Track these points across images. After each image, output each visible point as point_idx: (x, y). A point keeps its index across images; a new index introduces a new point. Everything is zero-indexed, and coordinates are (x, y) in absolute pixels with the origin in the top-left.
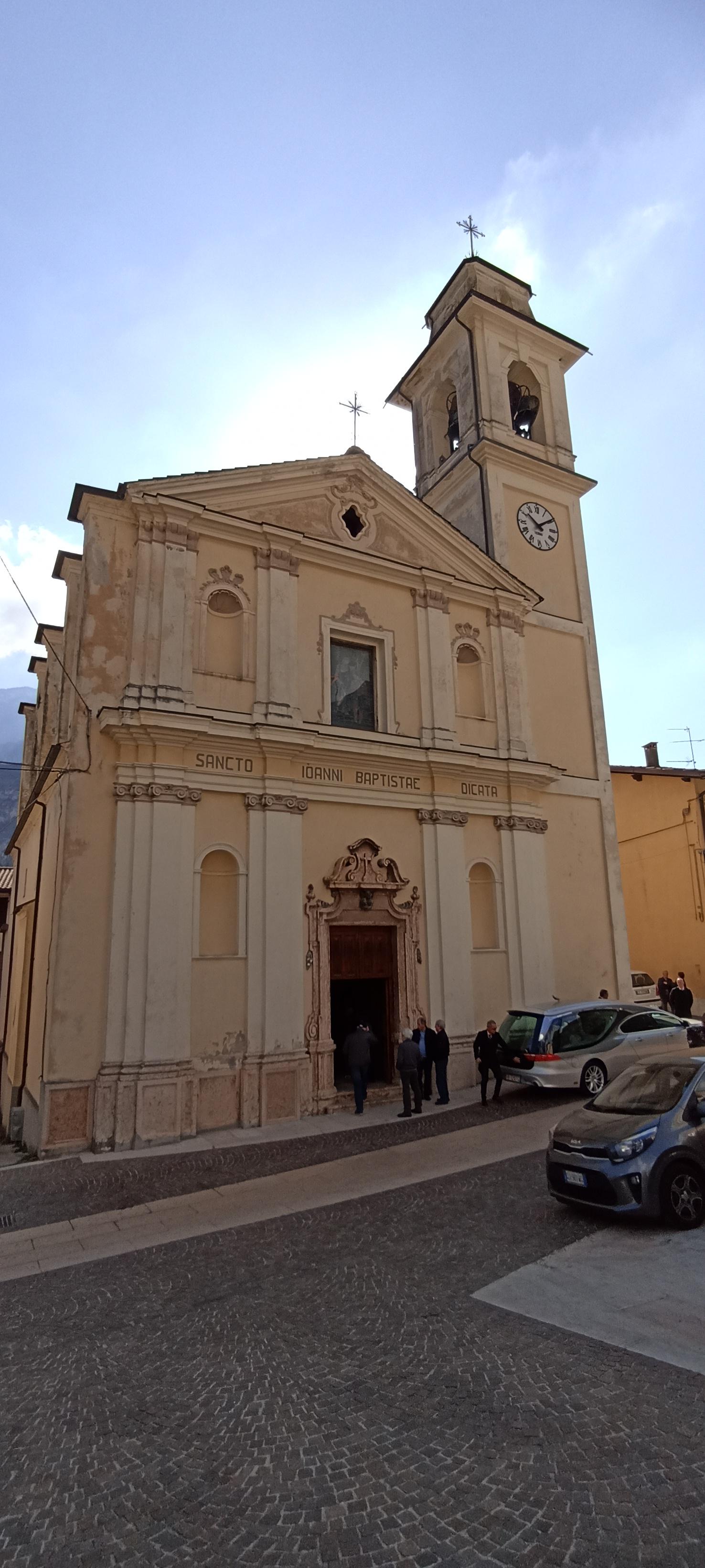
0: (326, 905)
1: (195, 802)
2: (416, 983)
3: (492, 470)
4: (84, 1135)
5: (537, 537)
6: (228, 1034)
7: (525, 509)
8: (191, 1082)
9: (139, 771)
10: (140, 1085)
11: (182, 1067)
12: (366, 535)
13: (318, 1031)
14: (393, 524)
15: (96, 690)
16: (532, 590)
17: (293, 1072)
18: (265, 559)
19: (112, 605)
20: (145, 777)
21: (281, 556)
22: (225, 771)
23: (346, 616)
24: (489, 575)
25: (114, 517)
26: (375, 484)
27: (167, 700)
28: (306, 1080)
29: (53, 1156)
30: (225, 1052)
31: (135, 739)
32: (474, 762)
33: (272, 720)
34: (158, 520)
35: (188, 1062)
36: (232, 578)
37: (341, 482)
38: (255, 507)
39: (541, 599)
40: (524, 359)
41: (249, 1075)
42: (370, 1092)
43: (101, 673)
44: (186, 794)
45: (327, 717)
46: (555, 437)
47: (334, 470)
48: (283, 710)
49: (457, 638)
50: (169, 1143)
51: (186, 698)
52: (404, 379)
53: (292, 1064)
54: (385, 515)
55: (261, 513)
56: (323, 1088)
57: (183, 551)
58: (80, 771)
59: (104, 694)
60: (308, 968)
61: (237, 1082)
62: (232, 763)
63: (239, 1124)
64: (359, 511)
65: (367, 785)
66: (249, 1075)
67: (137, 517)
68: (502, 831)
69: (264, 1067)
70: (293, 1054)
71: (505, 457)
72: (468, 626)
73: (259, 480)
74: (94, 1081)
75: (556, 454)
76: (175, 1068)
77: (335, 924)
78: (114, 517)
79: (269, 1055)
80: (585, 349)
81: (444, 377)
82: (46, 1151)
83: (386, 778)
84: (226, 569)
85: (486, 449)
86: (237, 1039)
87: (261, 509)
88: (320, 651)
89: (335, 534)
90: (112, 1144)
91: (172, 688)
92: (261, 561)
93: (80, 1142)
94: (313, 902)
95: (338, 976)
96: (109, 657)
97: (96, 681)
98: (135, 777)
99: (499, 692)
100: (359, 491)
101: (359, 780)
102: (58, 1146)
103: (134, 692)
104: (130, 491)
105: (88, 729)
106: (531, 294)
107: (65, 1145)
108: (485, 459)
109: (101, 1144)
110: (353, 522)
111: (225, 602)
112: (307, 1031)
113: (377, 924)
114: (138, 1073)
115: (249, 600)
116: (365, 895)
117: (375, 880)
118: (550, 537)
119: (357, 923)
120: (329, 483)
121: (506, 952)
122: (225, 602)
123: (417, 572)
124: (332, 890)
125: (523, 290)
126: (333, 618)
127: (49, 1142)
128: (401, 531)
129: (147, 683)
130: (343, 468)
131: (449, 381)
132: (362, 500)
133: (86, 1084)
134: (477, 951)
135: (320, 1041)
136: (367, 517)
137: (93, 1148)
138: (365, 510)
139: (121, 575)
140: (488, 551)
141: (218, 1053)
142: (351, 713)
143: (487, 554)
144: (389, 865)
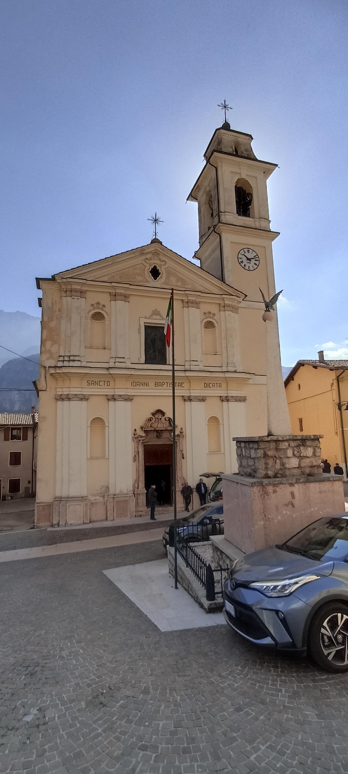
0: (142, 437)
1: (131, 400)
2: (182, 467)
3: (224, 235)
4: (50, 521)
5: (248, 265)
6: (102, 486)
7: (242, 252)
8: (87, 504)
9: (64, 389)
10: (68, 505)
11: (82, 499)
12: (161, 278)
13: (138, 485)
14: (174, 271)
15: (48, 359)
16: (241, 292)
17: (127, 501)
18: (114, 296)
19: (53, 324)
20: (66, 391)
21: (121, 295)
22: (99, 387)
23: (152, 316)
24: (220, 288)
25: (52, 288)
26: (164, 254)
27: (74, 361)
28: (132, 504)
29: (39, 528)
30: (101, 493)
31: (62, 377)
32: (208, 374)
33: (117, 365)
34: (69, 287)
35: (86, 497)
36: (101, 306)
37: (148, 256)
38: (111, 274)
39: (246, 296)
40: (244, 176)
41: (110, 502)
42: (156, 509)
43: (50, 351)
44: (82, 397)
45: (143, 359)
46: (259, 213)
47: (145, 252)
48: (122, 360)
49: (204, 319)
50: (79, 525)
51: (82, 359)
52: (192, 190)
53: (127, 498)
54: (170, 267)
55: (113, 276)
56: (140, 507)
57: (79, 299)
58: (43, 390)
59: (51, 360)
60: (134, 461)
61: (105, 504)
62: (102, 383)
63: (106, 519)
64: (158, 268)
65: (160, 387)
66: (110, 502)
67: (61, 287)
68: (224, 403)
69: (115, 499)
70: (128, 494)
71: (230, 229)
72: (210, 313)
73: (111, 263)
74: (52, 503)
75: (260, 222)
76: (81, 499)
77: (146, 444)
78: (52, 288)
79: (117, 495)
80: (277, 165)
81: (208, 190)
82: (37, 526)
83: (169, 384)
84: (98, 303)
85: (221, 227)
86: (106, 488)
87: (113, 274)
88: (139, 332)
89: (146, 280)
90: (58, 525)
91: (76, 356)
92: (222, 308)
93: (48, 523)
94: (136, 436)
95: (149, 464)
96: (52, 345)
97: (47, 355)
98: (63, 392)
99: (224, 341)
100: (158, 259)
101: (156, 385)
102: (40, 525)
103: (61, 359)
104: (57, 278)
105: (45, 374)
106: (252, 139)
107: (43, 524)
108: (221, 231)
109: (55, 525)
110: (155, 273)
111: (98, 316)
112: (134, 486)
113: (165, 443)
114: (67, 501)
115: (108, 315)
116: (159, 433)
117: (162, 425)
118: (255, 264)
119: (156, 443)
120: (143, 257)
121: (224, 454)
122: (209, 325)
123: (183, 292)
124: (145, 431)
125: (248, 138)
126: (145, 318)
127: (37, 523)
128: (178, 274)
129: (66, 355)
130: (149, 250)
131: (210, 191)
132: (159, 262)
133: (50, 504)
134: (211, 453)
135: (139, 489)
136: (162, 270)
137: (52, 526)
138: (160, 267)
139: (56, 311)
140: (222, 279)
141: (98, 493)
142: (155, 356)
143: (222, 281)
144: (169, 420)
